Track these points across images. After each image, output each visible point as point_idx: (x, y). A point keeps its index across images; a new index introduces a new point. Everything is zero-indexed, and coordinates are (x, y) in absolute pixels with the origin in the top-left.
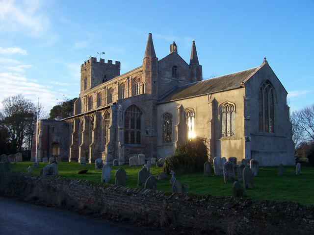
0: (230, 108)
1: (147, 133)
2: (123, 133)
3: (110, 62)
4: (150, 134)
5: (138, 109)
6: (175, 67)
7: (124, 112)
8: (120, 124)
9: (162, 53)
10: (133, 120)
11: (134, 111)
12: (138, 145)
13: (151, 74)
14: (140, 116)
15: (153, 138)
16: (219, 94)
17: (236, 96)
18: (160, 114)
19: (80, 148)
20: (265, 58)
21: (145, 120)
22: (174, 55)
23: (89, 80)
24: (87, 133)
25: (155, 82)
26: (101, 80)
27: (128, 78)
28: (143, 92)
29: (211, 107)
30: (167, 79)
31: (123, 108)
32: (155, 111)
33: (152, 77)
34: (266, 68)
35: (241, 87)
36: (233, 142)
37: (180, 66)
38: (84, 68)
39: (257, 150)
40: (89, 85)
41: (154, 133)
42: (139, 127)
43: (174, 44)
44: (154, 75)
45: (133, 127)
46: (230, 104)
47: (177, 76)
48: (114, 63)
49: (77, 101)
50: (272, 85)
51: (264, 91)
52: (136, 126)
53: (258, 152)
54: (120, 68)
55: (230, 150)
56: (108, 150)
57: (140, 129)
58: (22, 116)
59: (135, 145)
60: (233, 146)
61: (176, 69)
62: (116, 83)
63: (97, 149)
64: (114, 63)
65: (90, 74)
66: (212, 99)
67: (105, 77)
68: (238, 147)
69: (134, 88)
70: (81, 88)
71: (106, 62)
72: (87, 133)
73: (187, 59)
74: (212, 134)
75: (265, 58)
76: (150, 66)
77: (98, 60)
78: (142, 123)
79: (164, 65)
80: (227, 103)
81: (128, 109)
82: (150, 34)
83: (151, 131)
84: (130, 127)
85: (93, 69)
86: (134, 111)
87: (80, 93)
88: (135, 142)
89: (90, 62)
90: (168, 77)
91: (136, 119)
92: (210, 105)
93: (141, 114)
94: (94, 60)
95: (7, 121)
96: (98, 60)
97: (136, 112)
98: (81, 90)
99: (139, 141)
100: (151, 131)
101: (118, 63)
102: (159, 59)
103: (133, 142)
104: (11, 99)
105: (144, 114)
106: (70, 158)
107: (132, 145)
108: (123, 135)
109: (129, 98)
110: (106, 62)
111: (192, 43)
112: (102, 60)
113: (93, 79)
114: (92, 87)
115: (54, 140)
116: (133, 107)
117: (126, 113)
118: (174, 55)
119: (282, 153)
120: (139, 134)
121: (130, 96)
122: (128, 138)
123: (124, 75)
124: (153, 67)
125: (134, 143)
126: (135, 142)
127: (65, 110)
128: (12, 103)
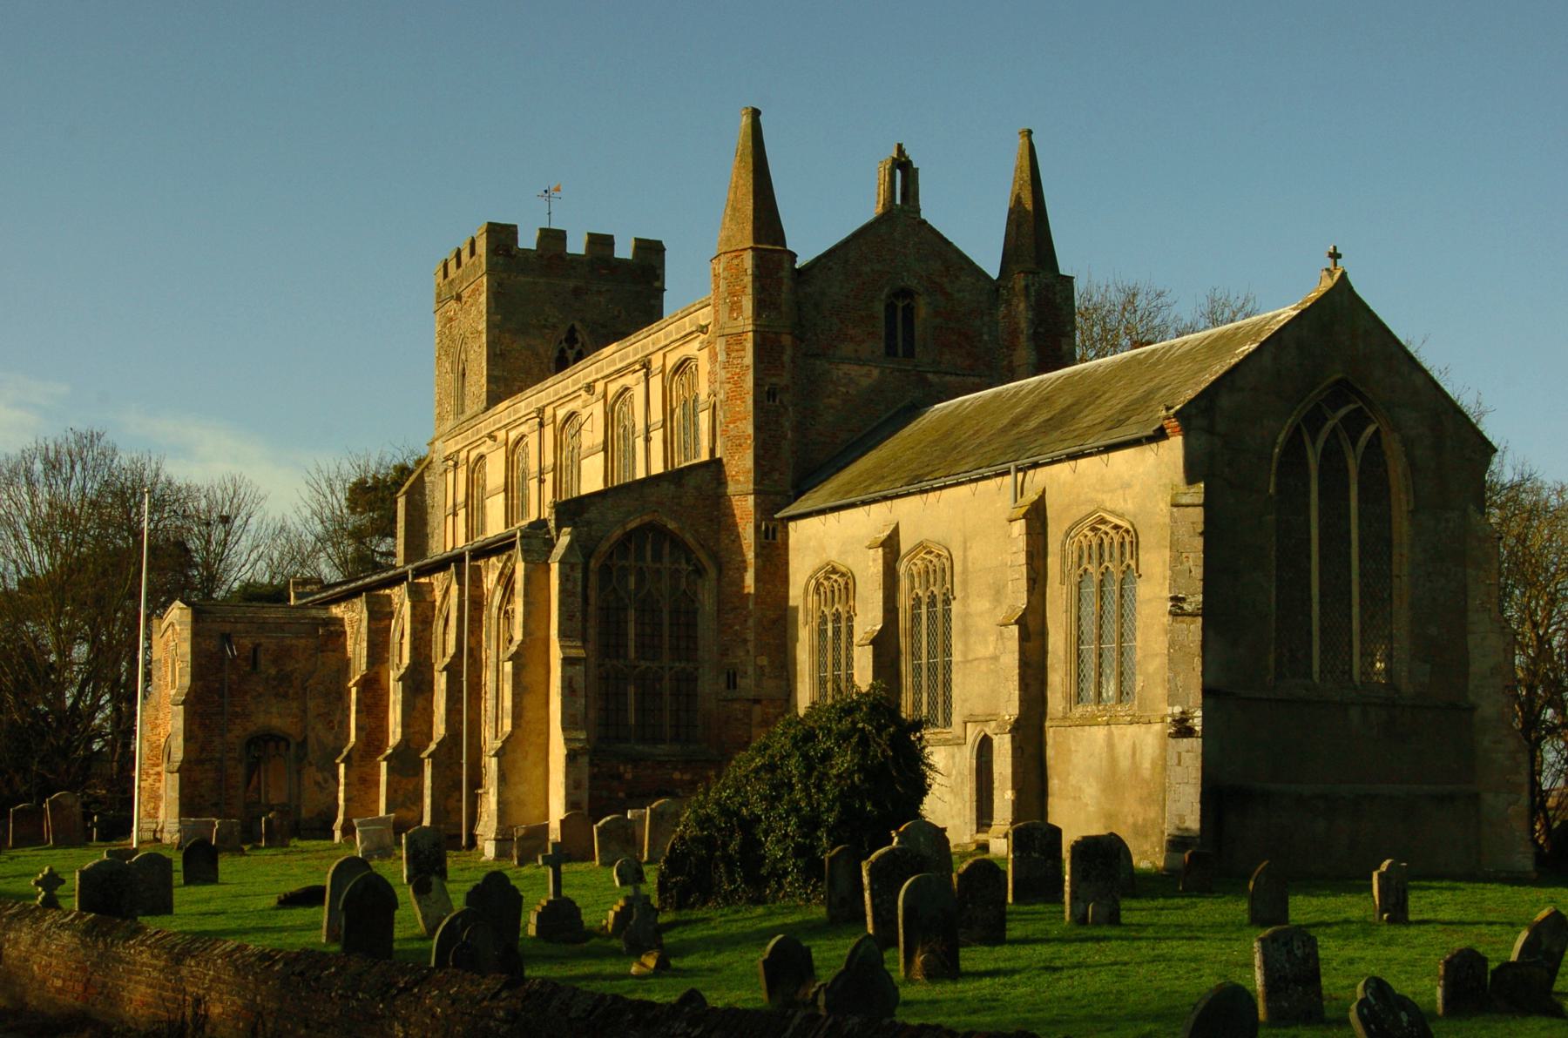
0: (1114, 545)
2: (580, 682)
3: (601, 243)
6: (906, 293)
11: (657, 557)
16: (1063, 470)
19: (384, 765)
22: (899, 229)
24: (418, 682)
27: (646, 365)
28: (712, 451)
29: (1021, 543)
30: (854, 370)
34: (1339, 319)
35: (1160, 435)
36: (1127, 735)
40: (478, 382)
43: (902, 164)
46: (1116, 527)
48: (624, 250)
55: (1112, 783)
57: (99, 839)
58: (125, 547)
60: (1123, 748)
61: (909, 312)
62: (589, 388)
64: (624, 250)
65: (483, 326)
66: (1031, 496)
67: (571, 338)
68: (1147, 764)
69: (272, 578)
71: (576, 245)
76: (747, 304)
77: (528, 240)
80: (1103, 521)
83: (750, 670)
84: (632, 654)
86: (657, 557)
89: (482, 247)
92: (1019, 527)
94: (501, 237)
95: (35, 595)
96: (528, 240)
100: (750, 670)
101: (650, 252)
102: (800, 262)
104: (38, 467)
109: (651, 480)
112: (553, 238)
114: (493, 399)
117: (606, 570)
118: (899, 229)
121: (657, 468)
128: (43, 494)
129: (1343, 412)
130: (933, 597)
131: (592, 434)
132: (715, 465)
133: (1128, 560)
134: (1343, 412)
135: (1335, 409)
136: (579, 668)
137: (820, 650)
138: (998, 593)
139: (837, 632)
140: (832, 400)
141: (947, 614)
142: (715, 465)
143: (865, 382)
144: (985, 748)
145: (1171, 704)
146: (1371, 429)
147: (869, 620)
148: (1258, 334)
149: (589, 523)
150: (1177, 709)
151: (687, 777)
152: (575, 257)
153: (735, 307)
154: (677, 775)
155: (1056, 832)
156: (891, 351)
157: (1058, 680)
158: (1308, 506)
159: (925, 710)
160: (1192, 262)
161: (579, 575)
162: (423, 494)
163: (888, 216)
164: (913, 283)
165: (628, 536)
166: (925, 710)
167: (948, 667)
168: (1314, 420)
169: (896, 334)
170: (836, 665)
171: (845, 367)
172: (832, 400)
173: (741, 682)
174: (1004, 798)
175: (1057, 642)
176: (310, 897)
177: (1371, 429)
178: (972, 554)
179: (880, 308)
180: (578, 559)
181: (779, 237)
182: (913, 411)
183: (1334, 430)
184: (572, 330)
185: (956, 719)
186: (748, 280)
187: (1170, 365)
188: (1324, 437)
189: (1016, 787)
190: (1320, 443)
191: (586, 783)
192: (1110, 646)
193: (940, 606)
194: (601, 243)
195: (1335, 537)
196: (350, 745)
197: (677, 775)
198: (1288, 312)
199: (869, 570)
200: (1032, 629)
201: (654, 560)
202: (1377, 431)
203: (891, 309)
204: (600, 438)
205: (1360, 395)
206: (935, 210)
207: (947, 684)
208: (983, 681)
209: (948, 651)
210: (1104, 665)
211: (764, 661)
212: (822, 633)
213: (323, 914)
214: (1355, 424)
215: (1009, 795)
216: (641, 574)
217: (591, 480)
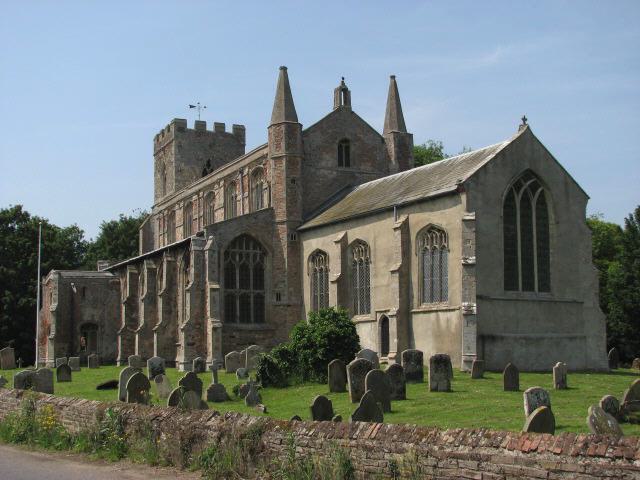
1: (279, 297)
2: (217, 298)
3: (220, 127)
4: (284, 300)
5: (257, 244)
6: (346, 141)
7: (222, 251)
8: (211, 279)
9: (312, 110)
10: (244, 268)
12: (257, 326)
13: (284, 162)
14: (262, 258)
15: (289, 309)
17: (452, 218)
18: (307, 253)
20: (524, 119)
21: (273, 267)
23: (171, 171)
24: (151, 300)
25: (293, 181)
26: (199, 170)
28: (269, 205)
29: (399, 237)
30: (326, 172)
31: (217, 244)
32: (295, 248)
33: (288, 168)
37: (359, 139)
38: (160, 151)
39: (498, 334)
41: (293, 298)
42: (259, 281)
44: (291, 164)
45: (244, 284)
47: (351, 163)
48: (229, 129)
49: (146, 220)
50: (541, 180)
51: (518, 199)
52: (252, 282)
53: (502, 338)
54: (244, 141)
55: (438, 335)
56: (186, 338)
59: (251, 326)
60: (443, 323)
61: (348, 148)
63: (170, 336)
64: (229, 129)
67: (209, 164)
70: (156, 191)
71: (210, 128)
72: (151, 300)
73: (377, 121)
74: (400, 297)
75: (524, 119)
76: (283, 144)
77: (191, 126)
78: (267, 276)
79: (318, 139)
81: (233, 243)
82: (284, 69)
83: (286, 293)
85: (179, 147)
87: (153, 204)
88: (252, 319)
89: (172, 129)
90: (328, 163)
91: (251, 267)
93: (265, 254)
94: (180, 125)
96: (191, 126)
97: (251, 251)
98: (156, 197)
99: (260, 318)
100: (286, 293)
101: (240, 131)
102: (304, 128)
103: (245, 318)
105: (270, 254)
106: (119, 358)
107: (244, 326)
108: (218, 303)
109: (246, 216)
110: (210, 128)
111: (389, 81)
112: (201, 125)
113: (179, 171)
115: (87, 318)
116: (244, 239)
117: (227, 253)
119: (571, 339)
120: (260, 299)
121: (247, 212)
122: (233, 309)
123: (254, 153)
124: (288, 146)
125: (249, 322)
126: (252, 319)
127: (122, 238)
129: (529, 183)
130: (361, 261)
131: (219, 200)
132: (270, 210)
133: (444, 243)
134: (529, 183)
135: (525, 182)
136: (217, 293)
137: (314, 285)
138: (389, 261)
139: (321, 277)
140: (318, 184)
141: (368, 269)
142: (270, 210)
143: (332, 176)
144: (385, 322)
145: (464, 301)
146: (540, 190)
147: (335, 272)
148: (494, 151)
149: (220, 234)
150: (466, 304)
151: (261, 337)
152: (209, 133)
153: (278, 146)
154: (257, 336)
155: (421, 354)
156: (340, 164)
157: (415, 292)
158: (515, 221)
159: (266, 202)
160: (461, 128)
161: (216, 255)
162: (149, 227)
163: (338, 111)
164: (348, 137)
165: (236, 239)
166: (266, 202)
167: (368, 290)
168: (517, 186)
169: (339, 156)
170: (321, 289)
171: (322, 171)
172: (318, 184)
173: (282, 298)
174: (393, 342)
175: (415, 278)
176: (112, 385)
177: (540, 190)
178: (379, 243)
179: (336, 147)
180: (216, 249)
181: (295, 118)
182: (349, 188)
183: (526, 190)
184: (209, 162)
185: (372, 310)
186: (283, 135)
187: (457, 166)
188: (524, 191)
189: (399, 338)
190: (520, 196)
191: (221, 340)
192: (436, 279)
193: (364, 265)
194: (220, 127)
195: (527, 231)
196: (123, 326)
197: (257, 336)
198: (506, 143)
199: (334, 252)
200: (404, 274)
201: (241, 287)
202: (542, 191)
203: (340, 147)
204: (222, 201)
205: (536, 176)
206: (357, 106)
207: (368, 296)
208: (384, 293)
209: (368, 282)
210: (436, 291)
211: (291, 289)
212: (315, 277)
213: (118, 393)
214: (534, 188)
215: (396, 340)
216: (241, 255)
217: (219, 217)
